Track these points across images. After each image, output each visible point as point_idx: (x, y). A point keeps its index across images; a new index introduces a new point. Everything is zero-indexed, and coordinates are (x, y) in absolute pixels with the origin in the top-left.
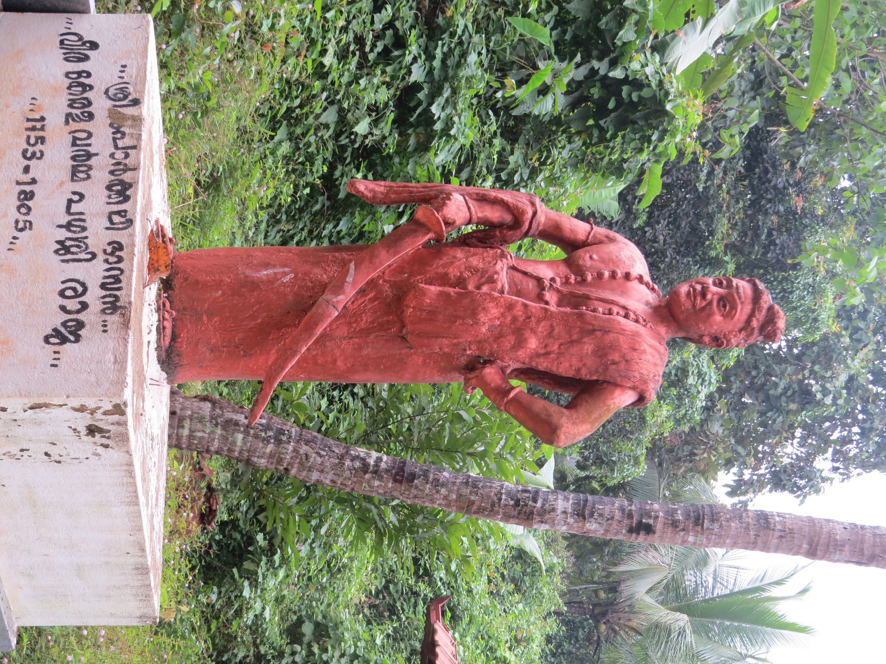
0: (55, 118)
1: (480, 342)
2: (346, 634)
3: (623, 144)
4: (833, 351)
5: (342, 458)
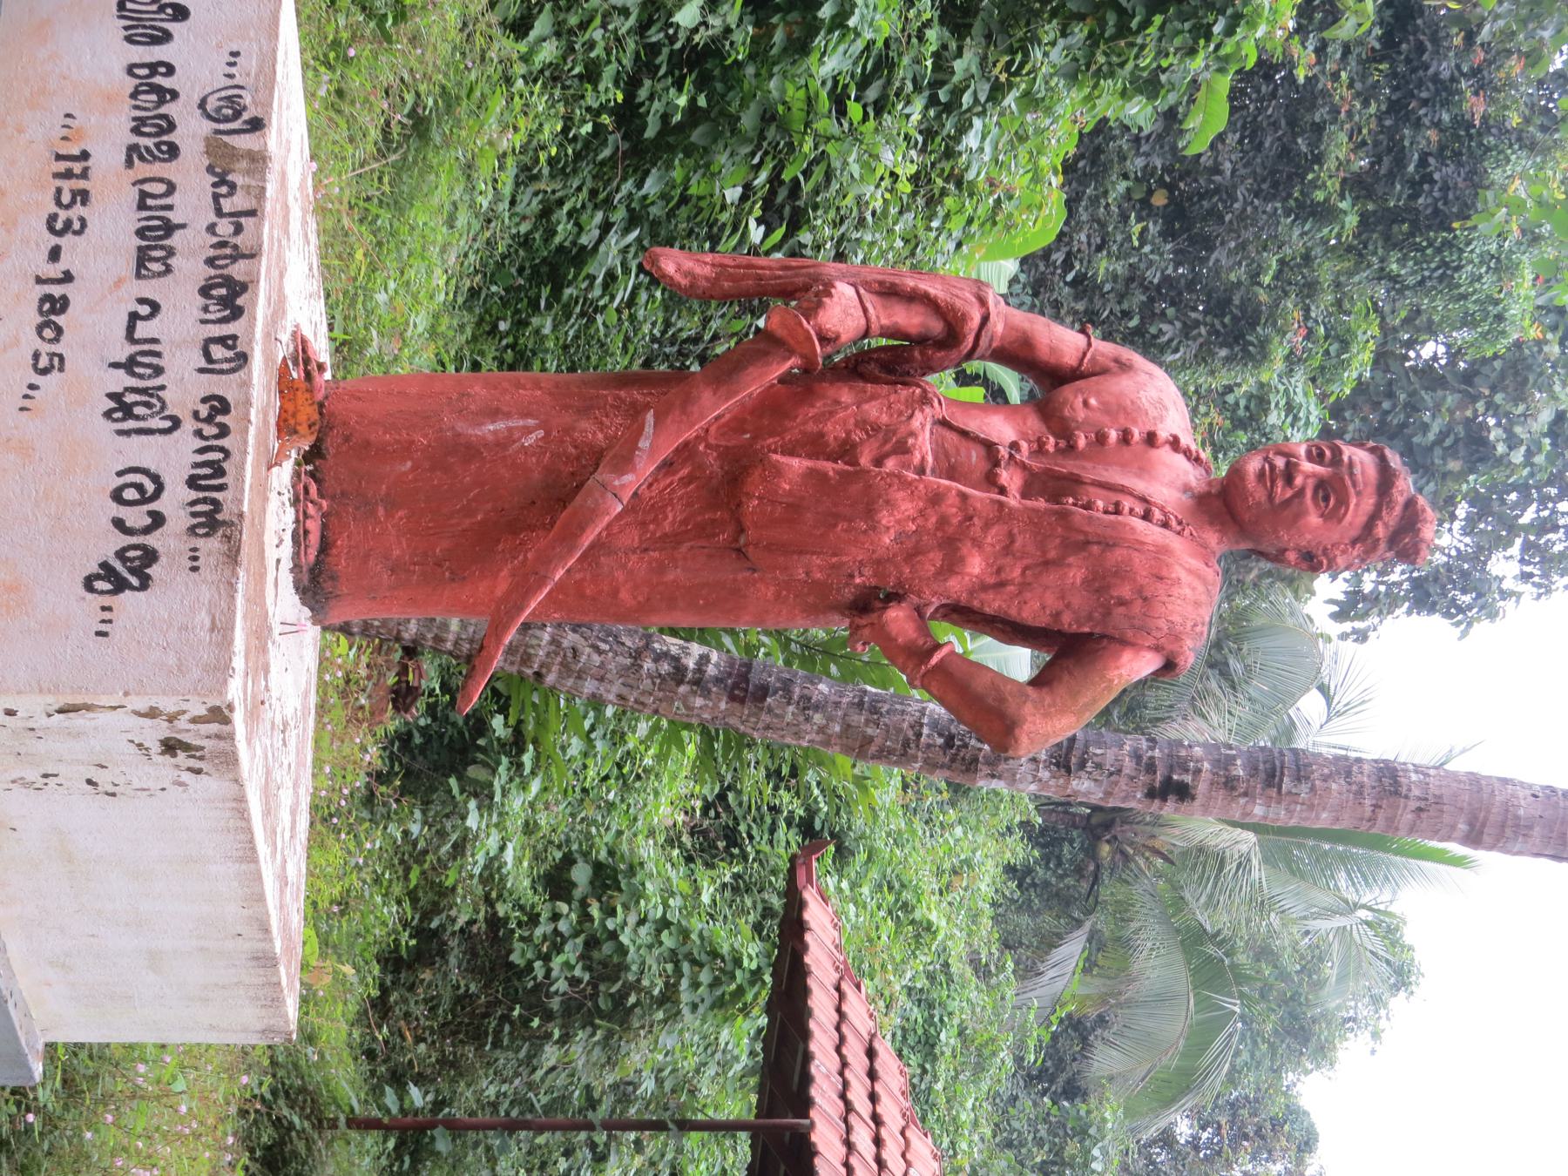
0: (107, 156)
1: (879, 562)
2: (648, 885)
3: (1160, 40)
4: (1529, 368)
5: (637, 655)
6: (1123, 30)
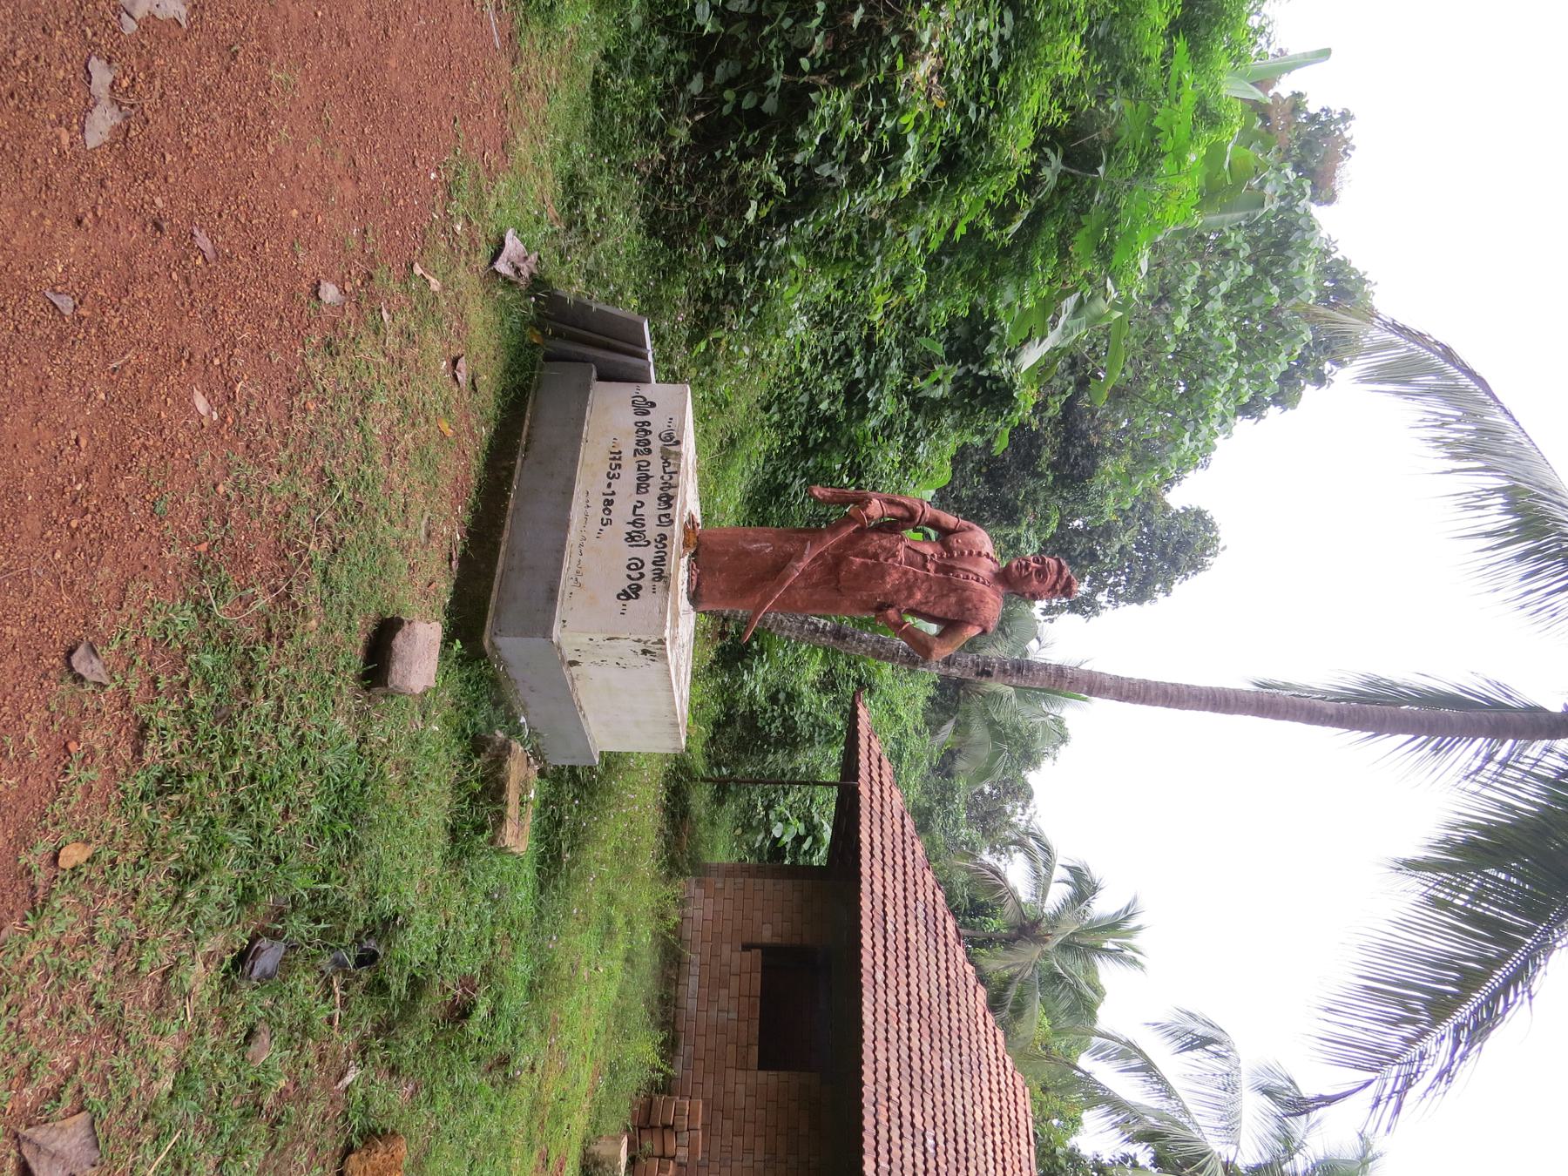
0: (628, 453)
5: (803, 623)
6: (973, 413)
